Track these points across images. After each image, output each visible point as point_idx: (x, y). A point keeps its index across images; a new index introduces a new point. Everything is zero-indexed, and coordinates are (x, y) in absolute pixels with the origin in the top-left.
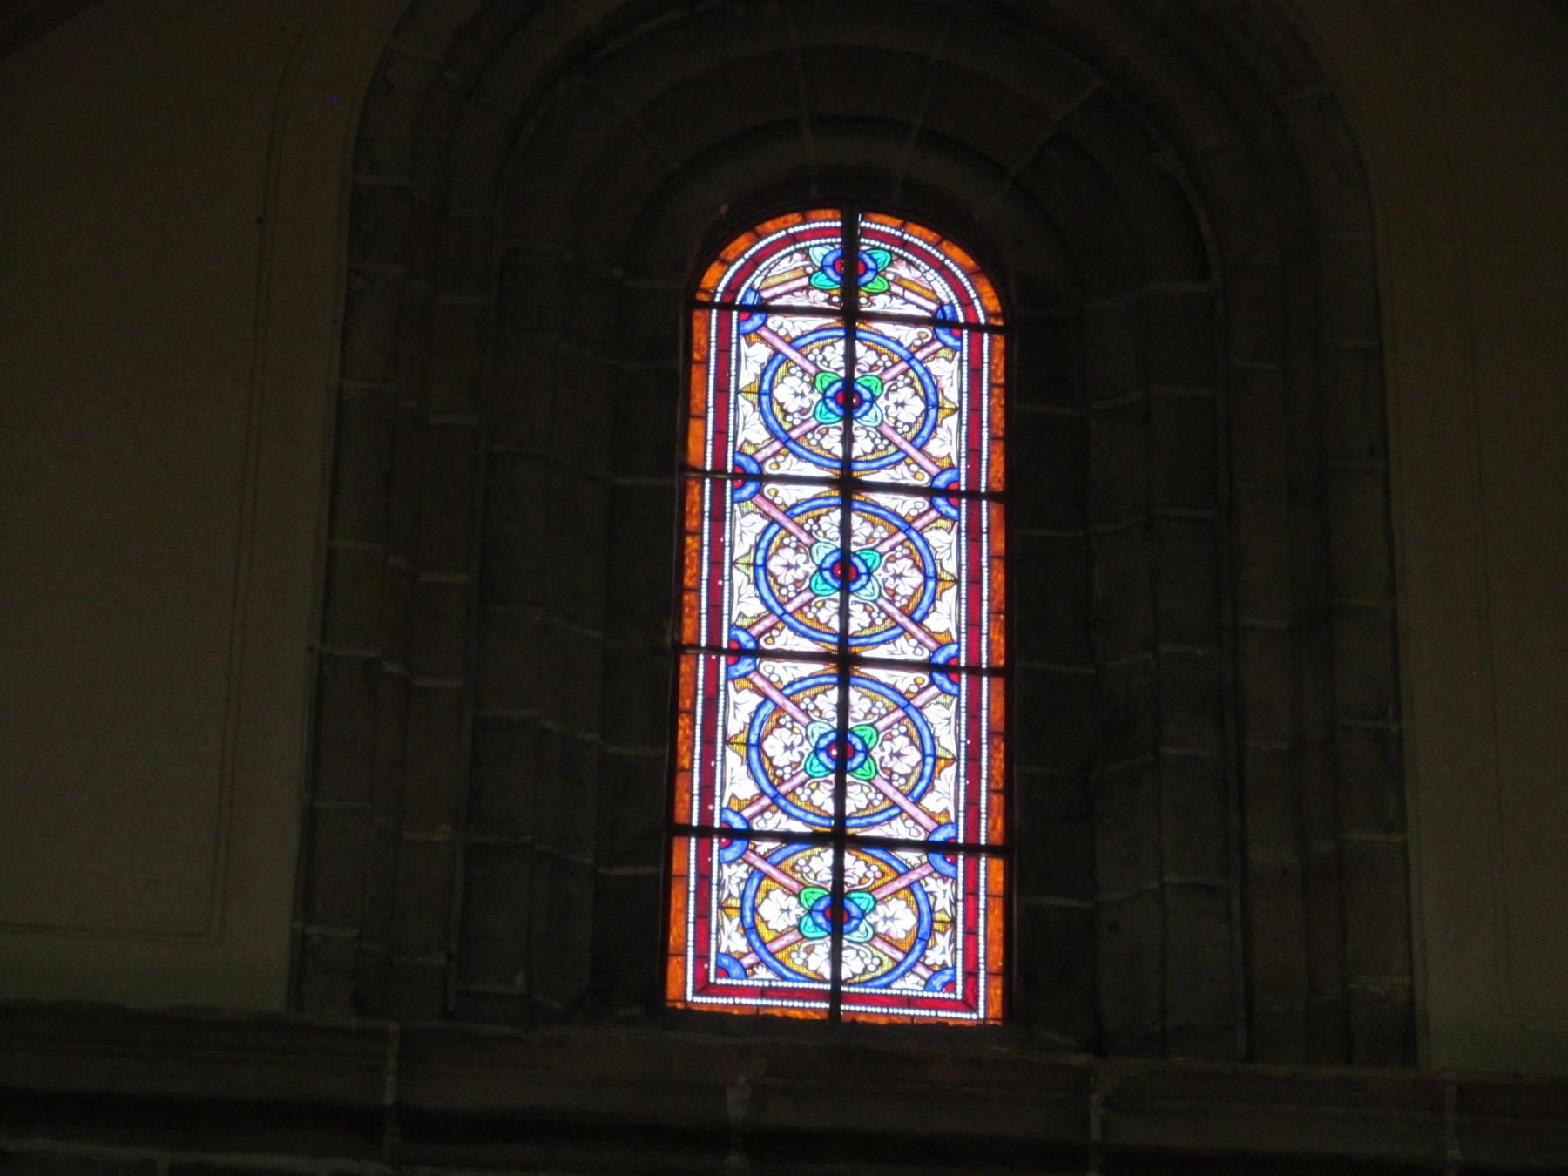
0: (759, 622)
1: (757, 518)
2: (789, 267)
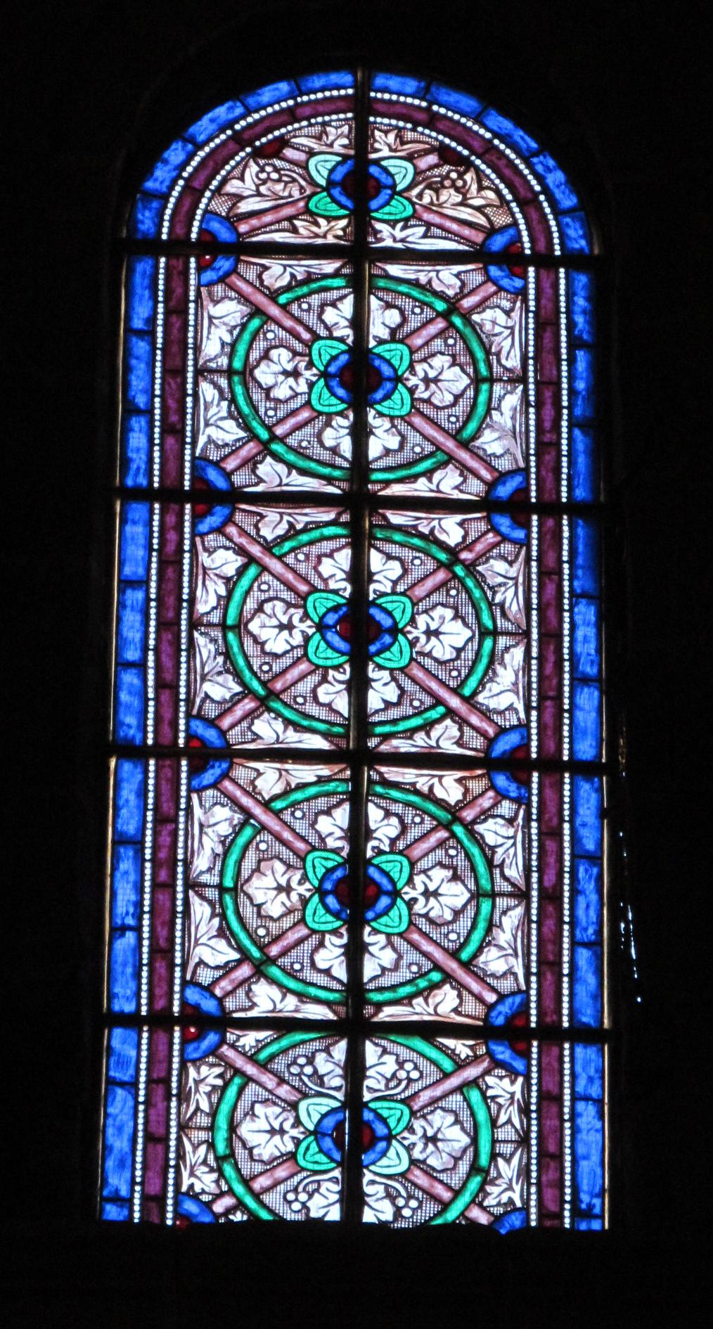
0: (229, 710)
1: (230, 555)
2: (267, 171)
